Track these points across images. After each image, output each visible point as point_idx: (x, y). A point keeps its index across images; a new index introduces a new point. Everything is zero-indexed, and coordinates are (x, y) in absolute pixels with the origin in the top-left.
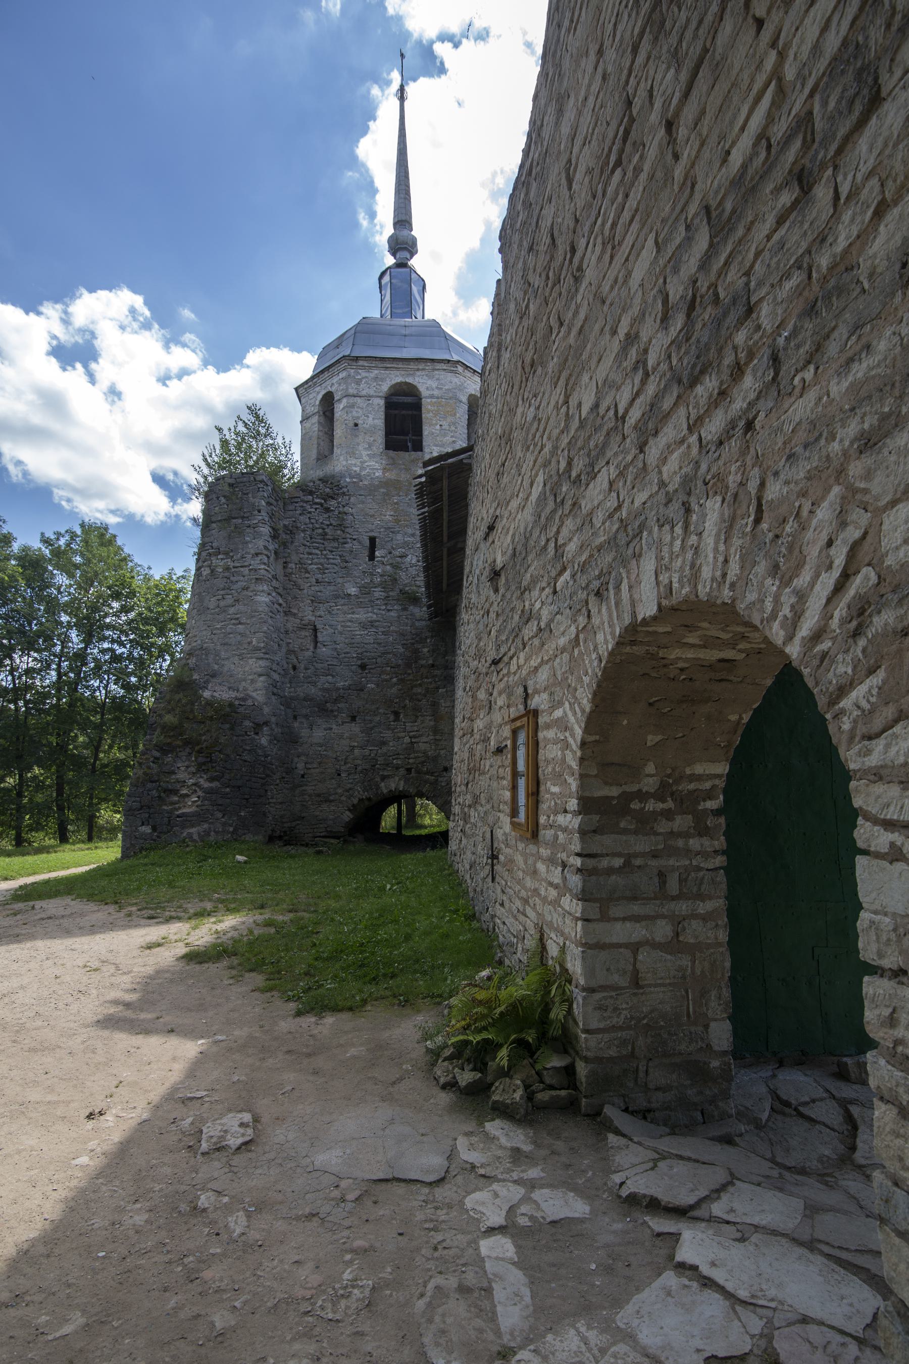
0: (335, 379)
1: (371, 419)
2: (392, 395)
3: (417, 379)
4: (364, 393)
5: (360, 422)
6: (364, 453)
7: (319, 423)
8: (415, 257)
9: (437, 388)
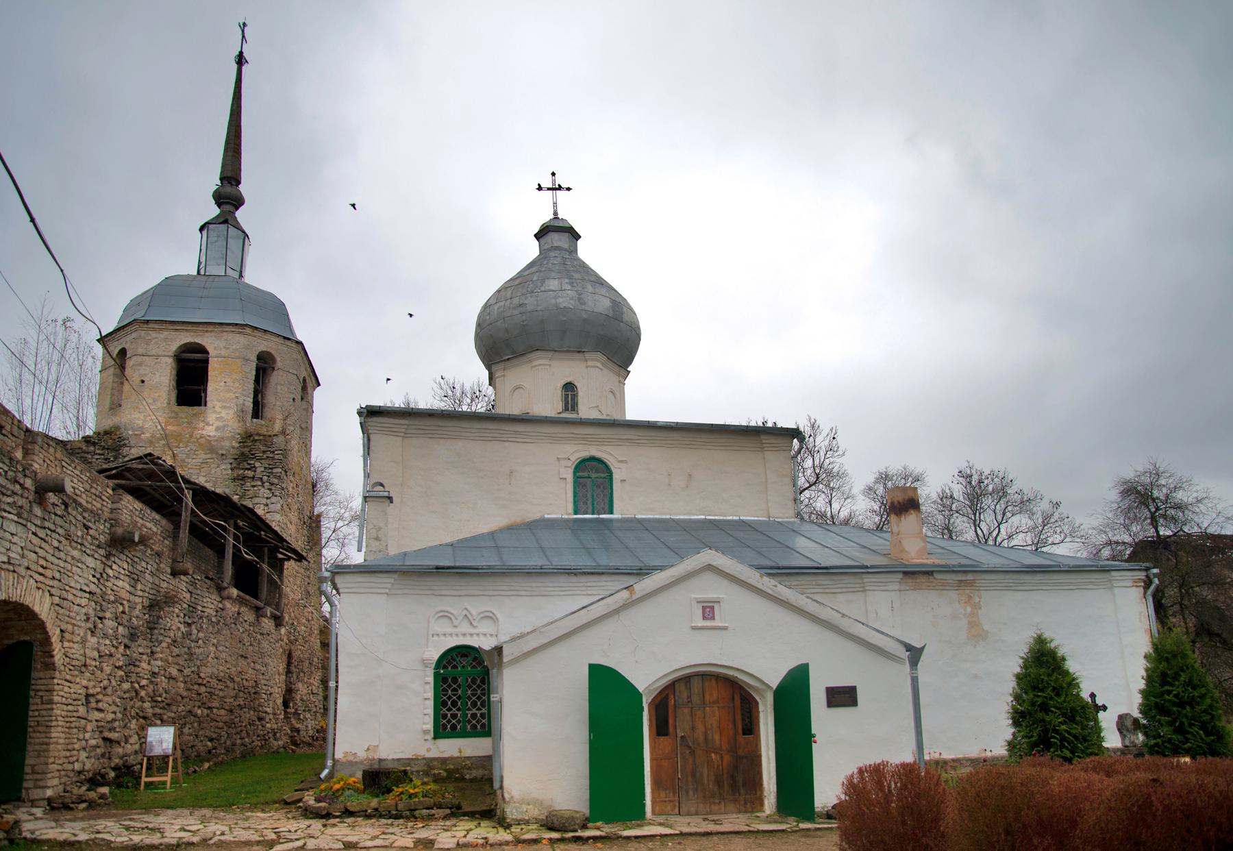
0: (129, 338)
1: (157, 376)
2: (184, 352)
3: (205, 339)
4: (153, 352)
5: (145, 379)
7: (114, 375)
8: (241, 209)
9: (224, 347)
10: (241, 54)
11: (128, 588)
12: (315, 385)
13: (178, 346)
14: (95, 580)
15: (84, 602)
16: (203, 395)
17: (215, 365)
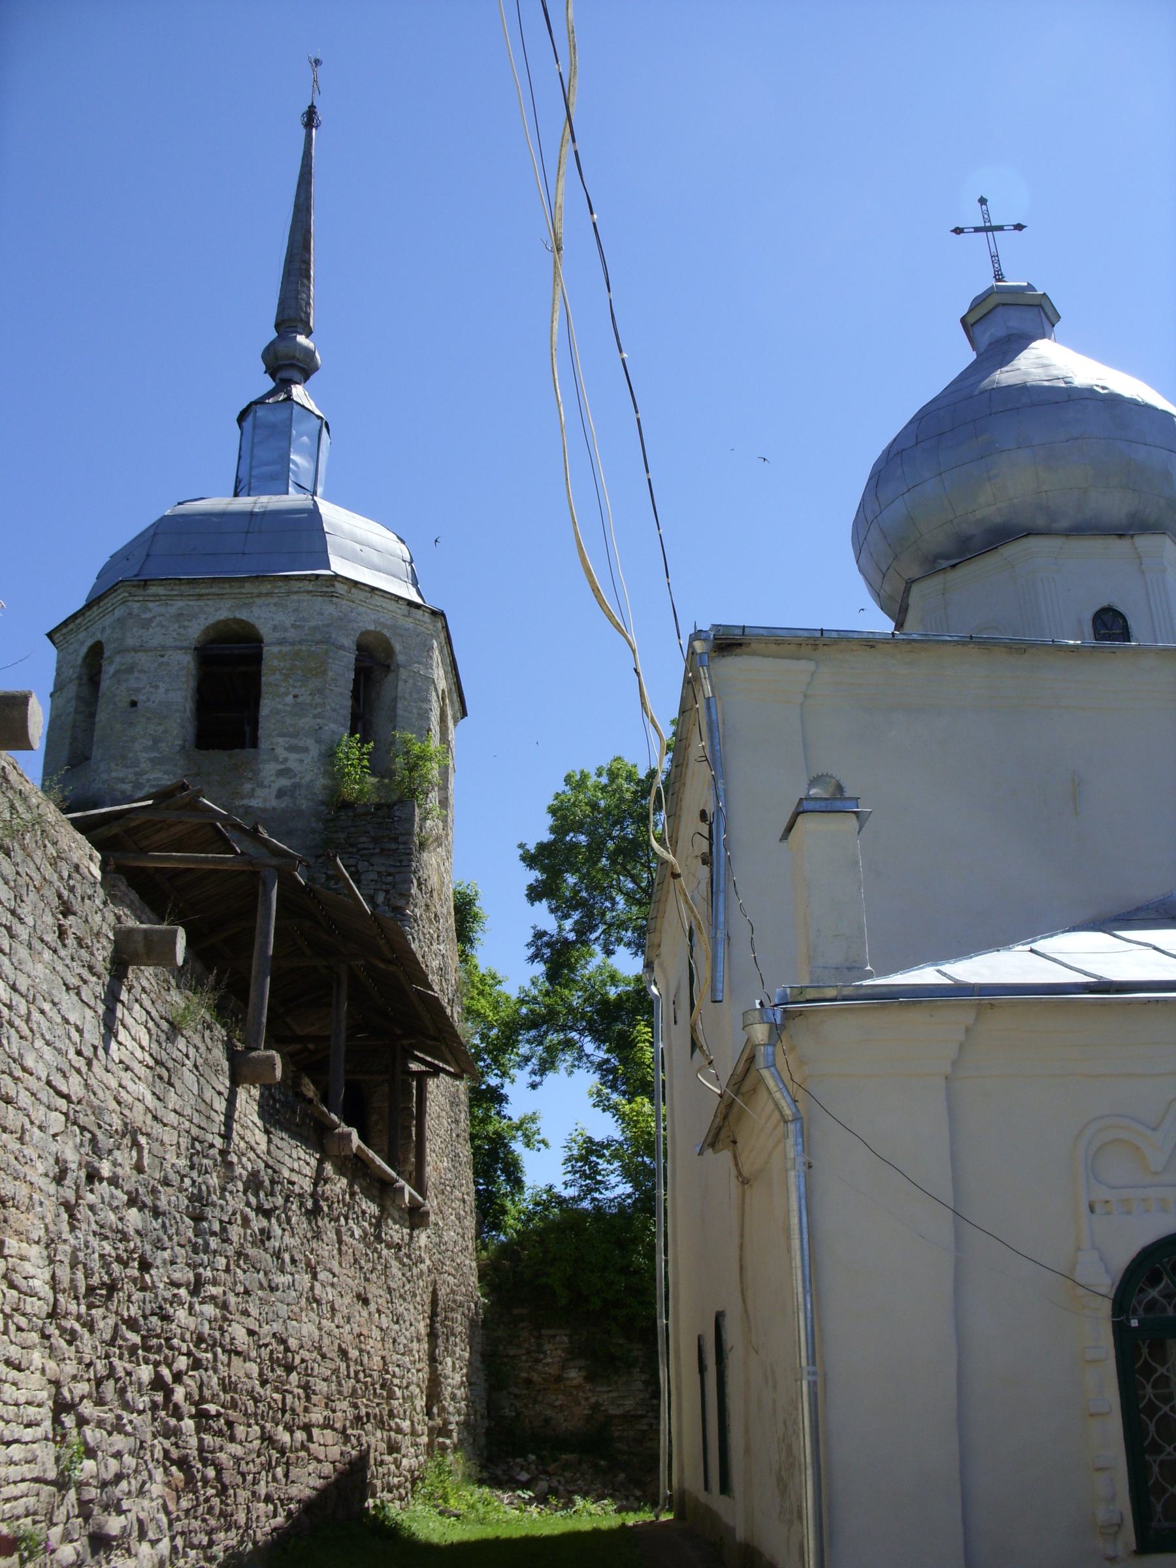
1: (162, 690)
2: (212, 641)
5: (141, 698)
6: (144, 756)
10: (311, 112)
11: (149, 1099)
12: (459, 715)
13: (202, 628)
14: (80, 1063)
15: (56, 1122)
16: (247, 729)
17: (276, 663)
